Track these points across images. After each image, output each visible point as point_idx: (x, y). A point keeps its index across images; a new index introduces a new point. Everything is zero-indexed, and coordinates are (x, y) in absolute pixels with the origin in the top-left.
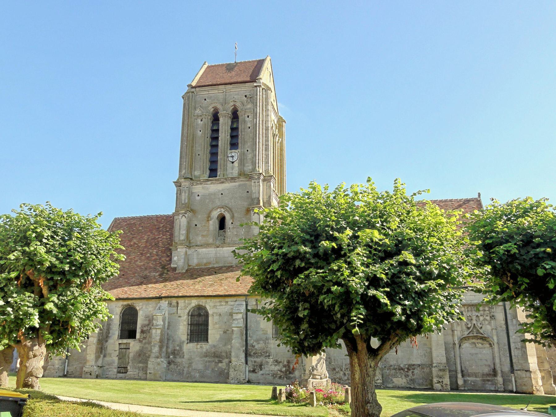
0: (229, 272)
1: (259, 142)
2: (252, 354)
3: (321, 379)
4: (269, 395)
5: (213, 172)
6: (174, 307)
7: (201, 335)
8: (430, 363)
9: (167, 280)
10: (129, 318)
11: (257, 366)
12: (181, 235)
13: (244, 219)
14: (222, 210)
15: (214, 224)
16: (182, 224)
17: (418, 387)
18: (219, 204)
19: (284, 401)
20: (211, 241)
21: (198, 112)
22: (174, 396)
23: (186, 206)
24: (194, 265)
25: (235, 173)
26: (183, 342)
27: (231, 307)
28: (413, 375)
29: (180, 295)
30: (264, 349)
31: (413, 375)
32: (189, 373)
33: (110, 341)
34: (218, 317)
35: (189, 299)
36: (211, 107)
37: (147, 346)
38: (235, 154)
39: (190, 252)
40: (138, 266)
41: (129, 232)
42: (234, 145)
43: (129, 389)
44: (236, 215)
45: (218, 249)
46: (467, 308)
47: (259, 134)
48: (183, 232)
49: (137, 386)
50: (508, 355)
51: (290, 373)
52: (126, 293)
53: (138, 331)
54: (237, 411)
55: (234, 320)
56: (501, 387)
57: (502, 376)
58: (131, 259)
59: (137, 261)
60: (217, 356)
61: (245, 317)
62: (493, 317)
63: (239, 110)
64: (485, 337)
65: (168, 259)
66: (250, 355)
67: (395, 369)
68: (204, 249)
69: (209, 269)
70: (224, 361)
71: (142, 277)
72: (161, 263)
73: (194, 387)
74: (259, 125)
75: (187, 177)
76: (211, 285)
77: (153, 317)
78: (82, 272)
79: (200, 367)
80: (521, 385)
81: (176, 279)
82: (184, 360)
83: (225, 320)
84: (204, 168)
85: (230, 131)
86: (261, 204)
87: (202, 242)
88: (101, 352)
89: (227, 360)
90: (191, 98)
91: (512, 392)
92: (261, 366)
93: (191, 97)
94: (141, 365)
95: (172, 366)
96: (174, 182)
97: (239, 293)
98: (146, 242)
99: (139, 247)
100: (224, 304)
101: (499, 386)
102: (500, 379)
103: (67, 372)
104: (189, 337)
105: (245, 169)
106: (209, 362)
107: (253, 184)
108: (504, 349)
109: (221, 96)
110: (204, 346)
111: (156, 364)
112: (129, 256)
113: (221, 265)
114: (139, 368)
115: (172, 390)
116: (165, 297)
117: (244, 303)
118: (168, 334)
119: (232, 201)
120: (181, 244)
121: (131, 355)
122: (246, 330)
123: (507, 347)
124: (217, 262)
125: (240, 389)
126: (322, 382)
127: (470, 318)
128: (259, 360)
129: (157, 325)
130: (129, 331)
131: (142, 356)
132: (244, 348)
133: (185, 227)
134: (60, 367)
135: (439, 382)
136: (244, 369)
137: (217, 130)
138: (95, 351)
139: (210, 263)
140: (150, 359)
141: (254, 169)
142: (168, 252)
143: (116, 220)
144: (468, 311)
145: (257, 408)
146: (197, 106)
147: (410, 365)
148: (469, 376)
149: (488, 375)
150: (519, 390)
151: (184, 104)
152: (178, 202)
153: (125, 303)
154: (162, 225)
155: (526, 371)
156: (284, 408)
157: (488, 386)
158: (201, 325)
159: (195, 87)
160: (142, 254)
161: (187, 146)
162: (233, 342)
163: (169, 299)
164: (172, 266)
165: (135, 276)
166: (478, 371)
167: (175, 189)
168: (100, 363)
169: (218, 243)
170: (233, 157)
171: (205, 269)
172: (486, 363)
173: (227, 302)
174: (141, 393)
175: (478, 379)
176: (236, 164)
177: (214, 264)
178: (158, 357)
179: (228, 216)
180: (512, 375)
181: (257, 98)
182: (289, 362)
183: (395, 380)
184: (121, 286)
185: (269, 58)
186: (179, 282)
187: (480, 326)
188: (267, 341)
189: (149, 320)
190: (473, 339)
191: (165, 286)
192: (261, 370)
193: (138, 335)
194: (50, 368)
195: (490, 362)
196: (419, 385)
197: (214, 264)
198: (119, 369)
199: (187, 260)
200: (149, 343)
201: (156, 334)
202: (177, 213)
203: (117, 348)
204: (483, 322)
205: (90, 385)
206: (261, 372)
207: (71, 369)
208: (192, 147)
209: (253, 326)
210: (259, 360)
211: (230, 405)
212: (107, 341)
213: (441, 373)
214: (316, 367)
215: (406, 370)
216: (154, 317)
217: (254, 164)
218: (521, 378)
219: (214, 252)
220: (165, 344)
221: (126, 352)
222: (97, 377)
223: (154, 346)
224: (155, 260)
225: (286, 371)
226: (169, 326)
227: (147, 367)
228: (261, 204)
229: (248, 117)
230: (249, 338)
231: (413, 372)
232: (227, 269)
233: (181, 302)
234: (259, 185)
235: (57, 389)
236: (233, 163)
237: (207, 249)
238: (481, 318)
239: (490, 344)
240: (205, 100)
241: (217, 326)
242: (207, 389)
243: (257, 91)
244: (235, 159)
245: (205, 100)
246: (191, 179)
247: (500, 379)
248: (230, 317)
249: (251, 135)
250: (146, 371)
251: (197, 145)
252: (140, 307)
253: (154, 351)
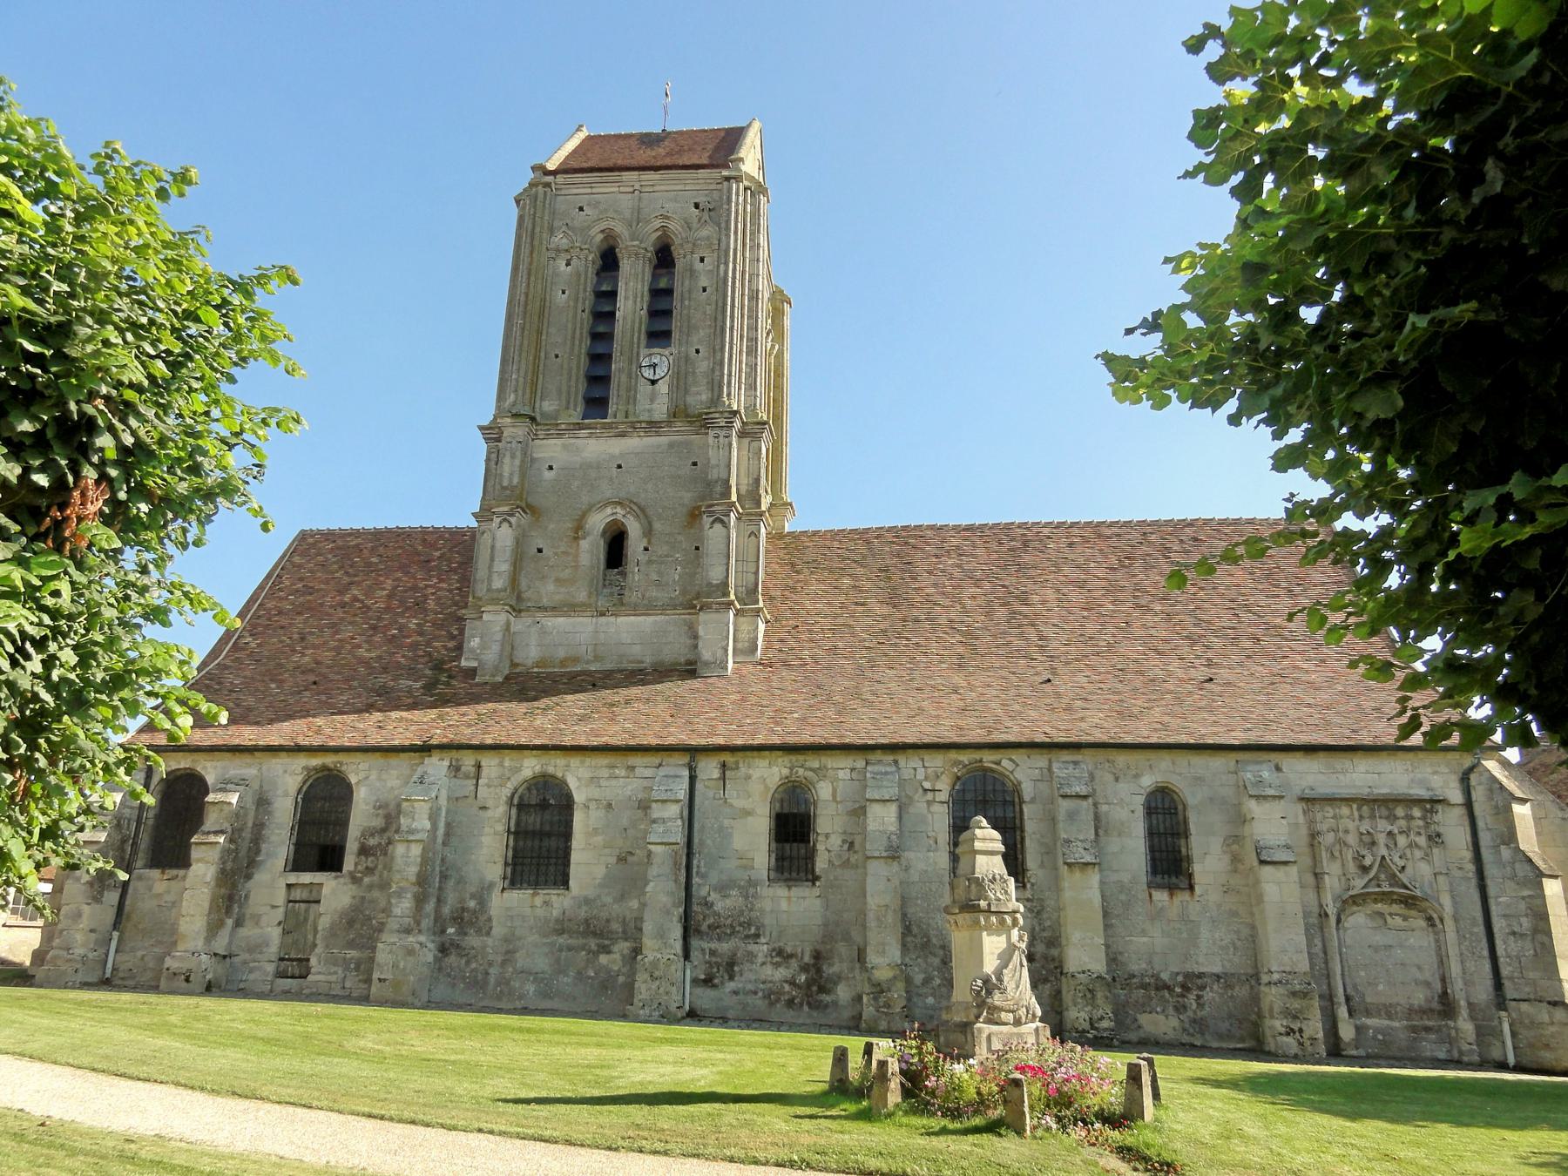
0: (635, 684)
1: (732, 328)
2: (704, 927)
3: (1017, 1022)
4: (823, 1072)
5: (596, 404)
6: (467, 777)
7: (548, 865)
8: (1250, 971)
9: (448, 701)
10: (325, 799)
11: (718, 965)
12: (495, 576)
13: (680, 538)
14: (618, 510)
15: (591, 550)
16: (498, 545)
17: (1215, 1045)
18: (608, 494)
19: (897, 1105)
20: (582, 596)
21: (559, 240)
22: (469, 1069)
23: (508, 495)
24: (530, 662)
25: (660, 410)
26: (491, 885)
27: (646, 783)
28: (1200, 1006)
29: (489, 741)
30: (742, 912)
31: (1200, 1006)
32: (503, 981)
33: (261, 877)
34: (601, 813)
35: (514, 754)
36: (597, 229)
37: (376, 894)
38: (661, 361)
39: (518, 625)
40: (361, 661)
41: (341, 568)
42: (659, 336)
43: (307, 1037)
44: (657, 526)
45: (603, 620)
46: (1359, 809)
47: (733, 306)
48: (503, 566)
49: (336, 1024)
50: (1486, 953)
51: (822, 990)
52: (319, 731)
53: (351, 847)
54: (732, 1152)
55: (654, 821)
56: (1471, 1052)
57: (1472, 1018)
58: (340, 640)
59: (359, 646)
60: (594, 931)
61: (686, 813)
62: (1435, 839)
63: (677, 241)
64: (1414, 898)
65: (451, 644)
66: (698, 932)
67: (1145, 986)
69: (573, 676)
70: (616, 948)
71: (372, 690)
72: (430, 654)
73: (529, 1031)
74: (734, 283)
75: (518, 417)
76: (583, 719)
77: (399, 806)
78: (34, 418)
79: (542, 963)
80: (1531, 1046)
81: (475, 699)
82: (490, 941)
83: (625, 822)
84: (569, 393)
85: (647, 298)
86: (734, 498)
87: (557, 597)
88: (228, 911)
89: (624, 947)
90: (541, 196)
91: (1502, 1066)
92: (730, 967)
93: (539, 200)
94: (353, 953)
95: (452, 959)
96: (481, 428)
97: (671, 741)
98: (390, 596)
99: (369, 608)
100: (623, 773)
101: (1465, 1047)
102: (1465, 1026)
103: (114, 969)
104: (509, 870)
105: (690, 400)
106: (570, 949)
107: (711, 440)
108: (1472, 934)
109: (626, 202)
110: (554, 898)
111: (402, 950)
112: (337, 633)
113: (609, 666)
114: (346, 963)
115: (455, 1044)
116: (442, 747)
117: (686, 773)
118: (443, 860)
119: (650, 486)
120: (495, 601)
121: (324, 923)
122: (689, 855)
123: (1480, 929)
124: (597, 658)
125: (682, 1041)
126: (1020, 1035)
127: (1366, 839)
128: (724, 947)
129: (411, 832)
130: (319, 849)
131: (357, 926)
132: (681, 910)
133: (508, 554)
134: (91, 955)
135: (1290, 1032)
136: (680, 974)
137: (612, 295)
138: (206, 905)
139: (576, 660)
140: (385, 937)
141: (716, 400)
142: (454, 625)
143: (303, 536)
144: (1361, 818)
145: (806, 1140)
146: (557, 224)
147: (1189, 976)
148: (1368, 1014)
149: (1424, 1012)
150: (1525, 1062)
151: (521, 219)
152: (490, 484)
153: (316, 761)
154: (437, 554)
155: (1554, 1004)
156: (898, 1136)
157: (1428, 1047)
158: (549, 835)
159: (554, 173)
160: (374, 628)
161: (523, 329)
162: (648, 889)
163: (454, 753)
164: (464, 663)
165: (351, 688)
166: (1395, 1000)
167: (483, 447)
168: (220, 945)
169: (602, 603)
170: (654, 366)
171: (563, 675)
172: (1419, 976)
173: (633, 768)
174: (347, 1054)
175: (1396, 1024)
176: (663, 387)
177: (587, 662)
178: (408, 931)
179: (634, 528)
180: (1503, 1014)
181: (729, 210)
182: (817, 956)
183: (1144, 1019)
184: (305, 713)
185: (756, 126)
186: (484, 708)
187: (1401, 863)
188: (752, 891)
189: (388, 817)
190: (1376, 901)
191: (440, 717)
192: (731, 978)
193: (349, 862)
194: (55, 957)
195: (1430, 974)
196: (1221, 1037)
197: (587, 662)
198: (283, 964)
199: (508, 648)
200: (384, 886)
201: (407, 857)
202: (484, 514)
203: (280, 897)
204: (1408, 852)
205: (173, 1019)
206: (731, 986)
207: (128, 961)
208: (539, 332)
209: (709, 842)
210: (724, 947)
211: (692, 1118)
212: (249, 877)
213: (1296, 1004)
214: (1000, 980)
215: (1178, 990)
216: (405, 804)
217: (716, 386)
218: (1534, 1024)
219: (591, 629)
220: (433, 891)
221: (307, 911)
222: (209, 989)
223: (399, 894)
224: (414, 646)
225: (809, 984)
226: (447, 834)
227: (372, 960)
228: (734, 498)
229: (702, 260)
230: (696, 880)
231: (1199, 997)
232: (627, 677)
233: (490, 762)
234: (730, 445)
235: (49, 1031)
236: (653, 382)
237: (571, 620)
238: (1402, 841)
239: (1429, 919)
240: (581, 209)
241: (599, 839)
242: (574, 1039)
243: (730, 189)
244: (660, 372)
245: (581, 209)
246: (533, 419)
247: (1465, 1026)
248: (640, 813)
249: (709, 309)
250: (370, 972)
251: (553, 330)
252: (362, 775)
253: (397, 911)
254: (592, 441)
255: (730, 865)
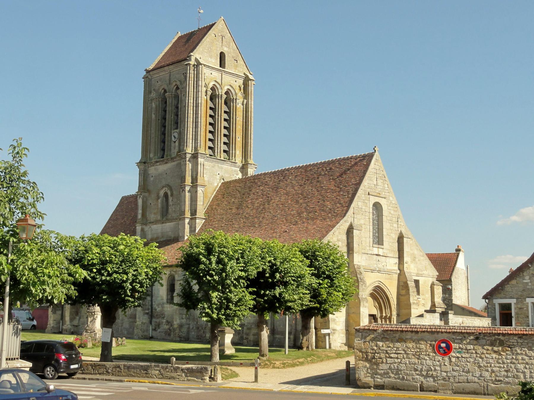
23: (144, 186)
45: (163, 224)
68: (155, 226)
124: (163, 237)
128: (158, 320)
210: (158, 320)
254: (160, 166)
255: (159, 298)
